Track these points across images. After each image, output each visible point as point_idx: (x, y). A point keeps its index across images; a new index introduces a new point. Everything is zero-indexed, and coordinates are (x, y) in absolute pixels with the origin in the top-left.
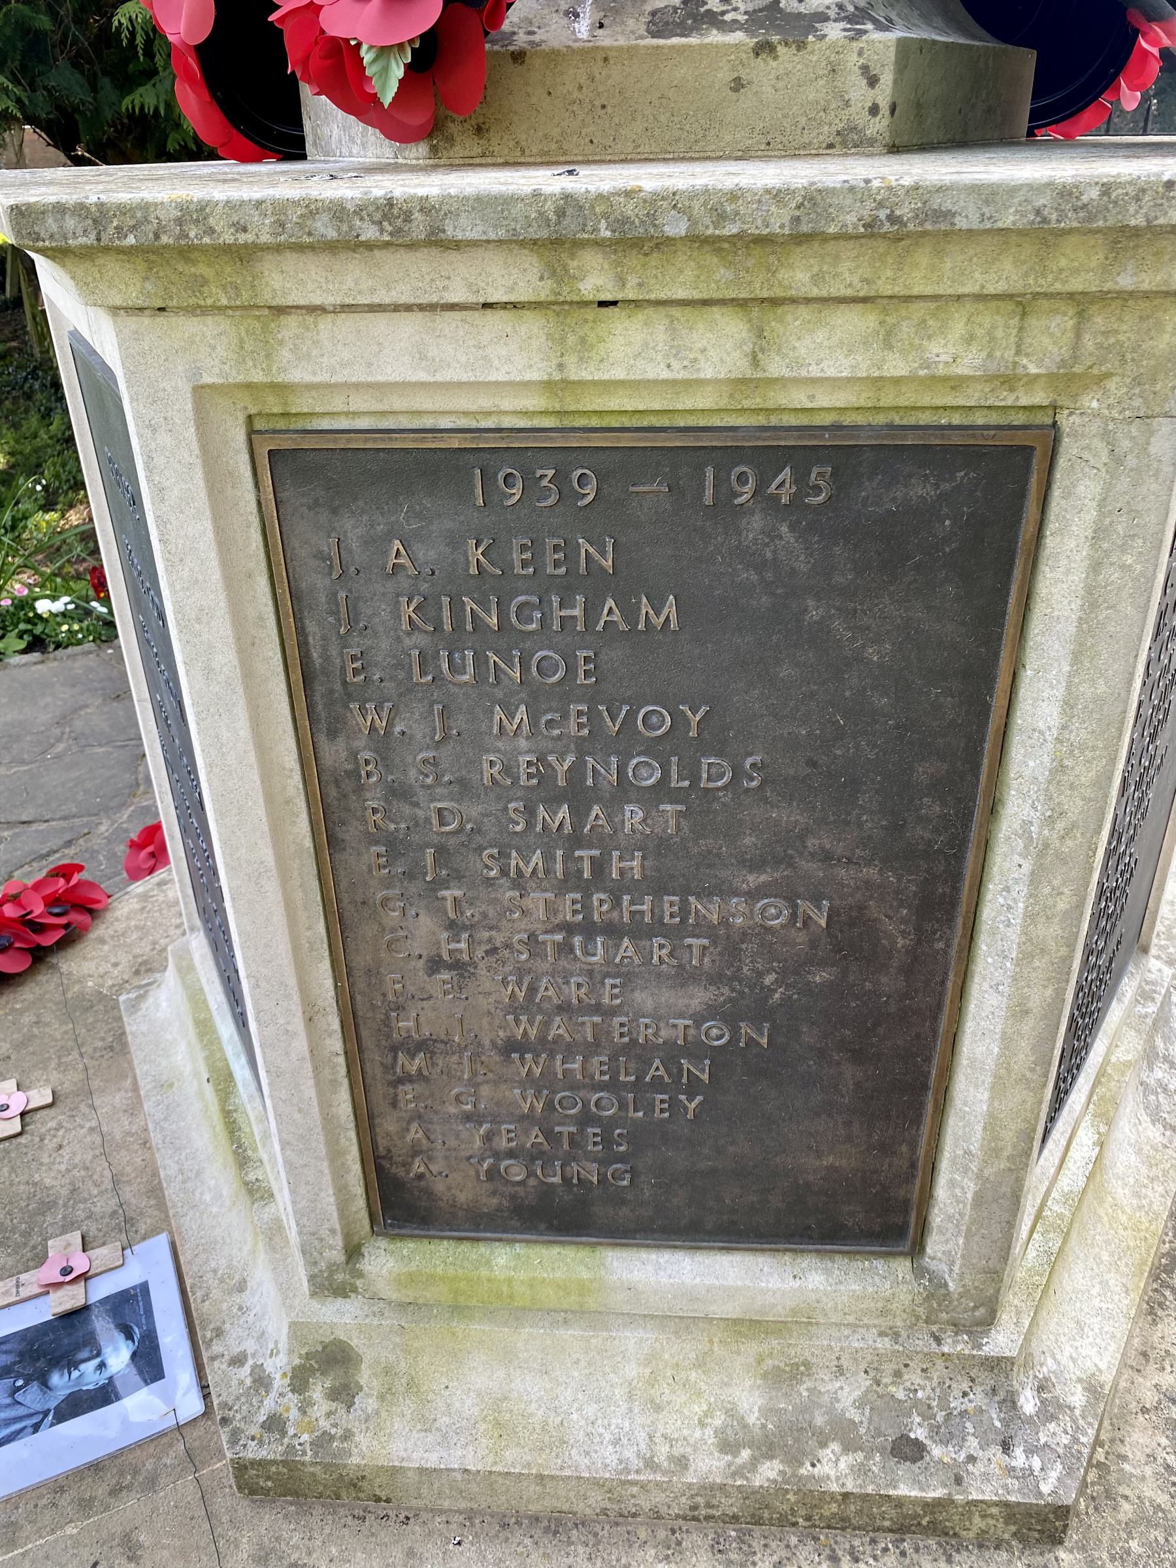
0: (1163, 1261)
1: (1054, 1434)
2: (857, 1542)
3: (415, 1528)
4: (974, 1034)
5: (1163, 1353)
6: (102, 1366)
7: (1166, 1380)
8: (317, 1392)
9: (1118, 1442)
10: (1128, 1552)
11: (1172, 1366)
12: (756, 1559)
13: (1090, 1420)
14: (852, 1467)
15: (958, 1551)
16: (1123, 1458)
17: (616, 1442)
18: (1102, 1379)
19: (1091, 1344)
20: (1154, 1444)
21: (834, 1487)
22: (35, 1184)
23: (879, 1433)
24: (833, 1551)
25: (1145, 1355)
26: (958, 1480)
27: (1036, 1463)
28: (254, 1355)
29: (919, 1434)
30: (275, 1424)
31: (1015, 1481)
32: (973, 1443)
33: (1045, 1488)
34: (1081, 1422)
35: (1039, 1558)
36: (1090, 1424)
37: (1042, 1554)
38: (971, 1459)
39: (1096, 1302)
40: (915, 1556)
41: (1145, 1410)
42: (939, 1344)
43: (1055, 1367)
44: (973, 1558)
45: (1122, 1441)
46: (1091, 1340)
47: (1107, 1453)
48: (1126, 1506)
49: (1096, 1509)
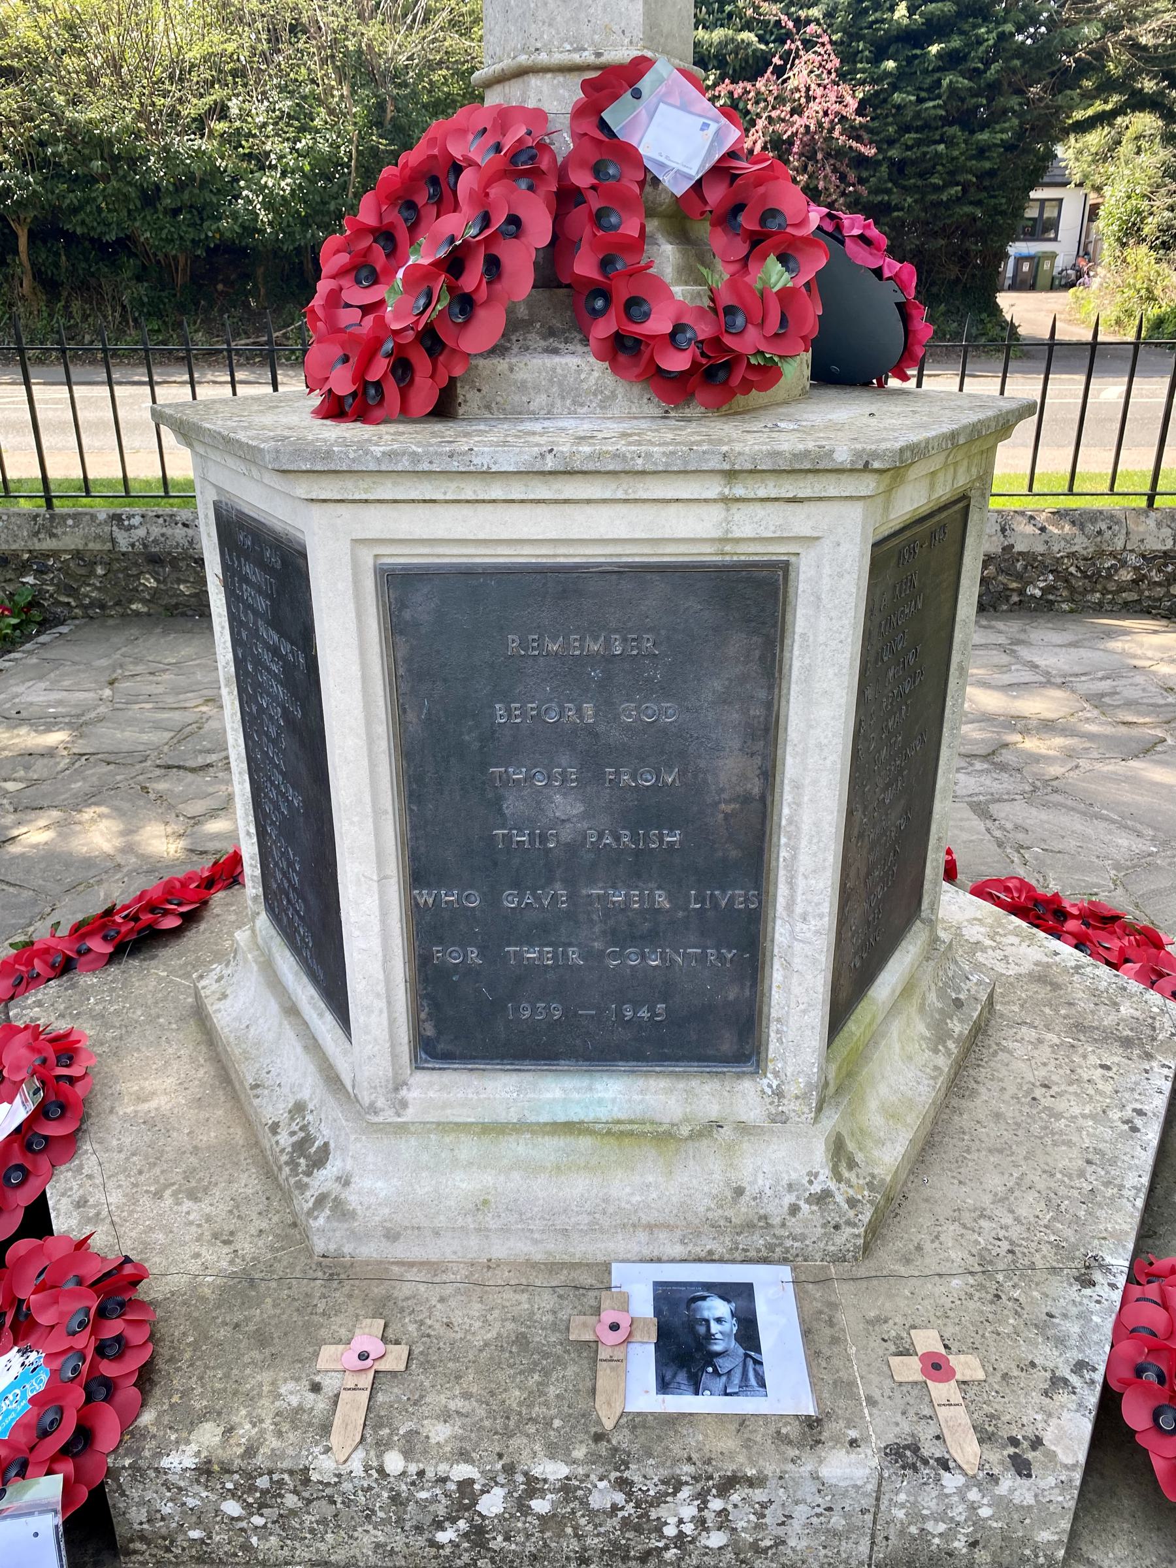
3: (910, 1195)
4: (964, 643)
6: (719, 1320)
8: (846, 1174)
22: (486, 1345)
28: (798, 1198)
30: (852, 1203)
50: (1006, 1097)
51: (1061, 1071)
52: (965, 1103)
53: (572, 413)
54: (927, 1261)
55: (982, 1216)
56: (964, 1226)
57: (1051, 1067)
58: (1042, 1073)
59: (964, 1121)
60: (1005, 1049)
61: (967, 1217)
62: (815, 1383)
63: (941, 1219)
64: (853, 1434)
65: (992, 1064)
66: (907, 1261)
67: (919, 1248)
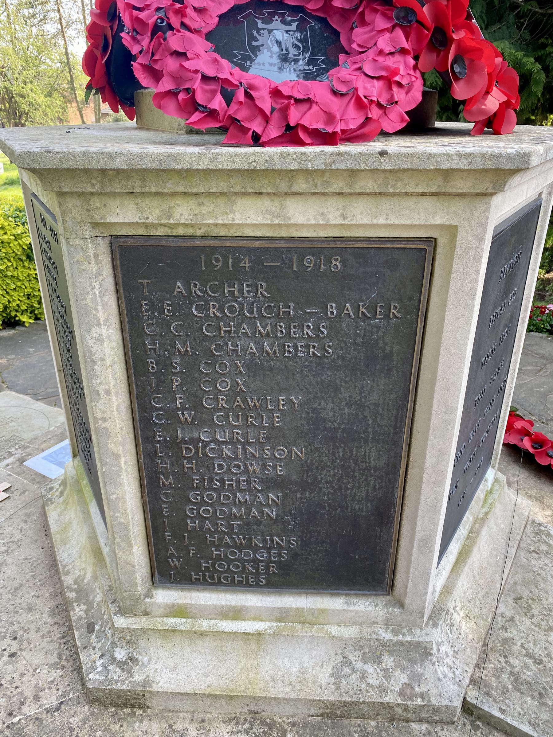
0: (268, 720)
1: (116, 673)
2: (71, 642)
3: (44, 538)
5: (207, 729)
7: (192, 732)
9: (149, 718)
10: (95, 731)
11: (201, 734)
12: (57, 617)
13: (130, 685)
14: (80, 615)
15: (78, 672)
16: (141, 721)
17: (69, 555)
18: (154, 686)
19: (169, 677)
20: (154, 733)
21: (71, 614)
23: (92, 616)
24: (67, 636)
25: (203, 721)
26: (85, 648)
27: (100, 669)
29: (97, 627)
31: (90, 665)
32: (99, 645)
33: (91, 676)
34: (127, 682)
35: (83, 700)
36: (128, 686)
37: (84, 700)
38: (94, 648)
39: (193, 674)
40: (71, 660)
41: (170, 726)
42: (111, 603)
43: (146, 663)
44: (76, 678)
45: (150, 720)
46: (171, 676)
47: (141, 715)
48: (117, 727)
49: (112, 716)
50: (32, 626)
51: (8, 678)
52: (53, 603)
53: (271, 158)
54: (19, 520)
55: (7, 551)
56: (12, 542)
57: (16, 676)
58: (21, 664)
59: (47, 592)
60: (55, 666)
61: (15, 546)
62: (30, 469)
63: (24, 538)
64: (9, 467)
65: (56, 645)
66: (26, 515)
67: (26, 522)
